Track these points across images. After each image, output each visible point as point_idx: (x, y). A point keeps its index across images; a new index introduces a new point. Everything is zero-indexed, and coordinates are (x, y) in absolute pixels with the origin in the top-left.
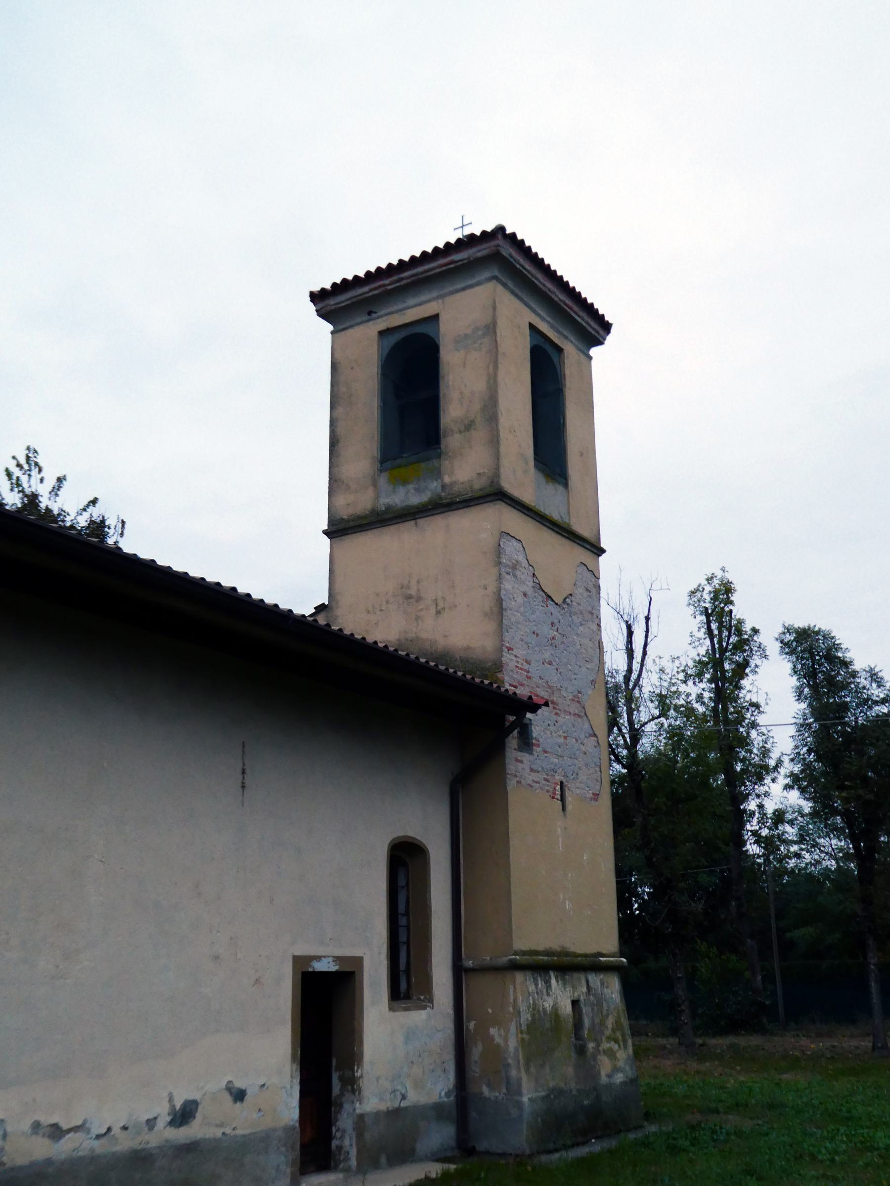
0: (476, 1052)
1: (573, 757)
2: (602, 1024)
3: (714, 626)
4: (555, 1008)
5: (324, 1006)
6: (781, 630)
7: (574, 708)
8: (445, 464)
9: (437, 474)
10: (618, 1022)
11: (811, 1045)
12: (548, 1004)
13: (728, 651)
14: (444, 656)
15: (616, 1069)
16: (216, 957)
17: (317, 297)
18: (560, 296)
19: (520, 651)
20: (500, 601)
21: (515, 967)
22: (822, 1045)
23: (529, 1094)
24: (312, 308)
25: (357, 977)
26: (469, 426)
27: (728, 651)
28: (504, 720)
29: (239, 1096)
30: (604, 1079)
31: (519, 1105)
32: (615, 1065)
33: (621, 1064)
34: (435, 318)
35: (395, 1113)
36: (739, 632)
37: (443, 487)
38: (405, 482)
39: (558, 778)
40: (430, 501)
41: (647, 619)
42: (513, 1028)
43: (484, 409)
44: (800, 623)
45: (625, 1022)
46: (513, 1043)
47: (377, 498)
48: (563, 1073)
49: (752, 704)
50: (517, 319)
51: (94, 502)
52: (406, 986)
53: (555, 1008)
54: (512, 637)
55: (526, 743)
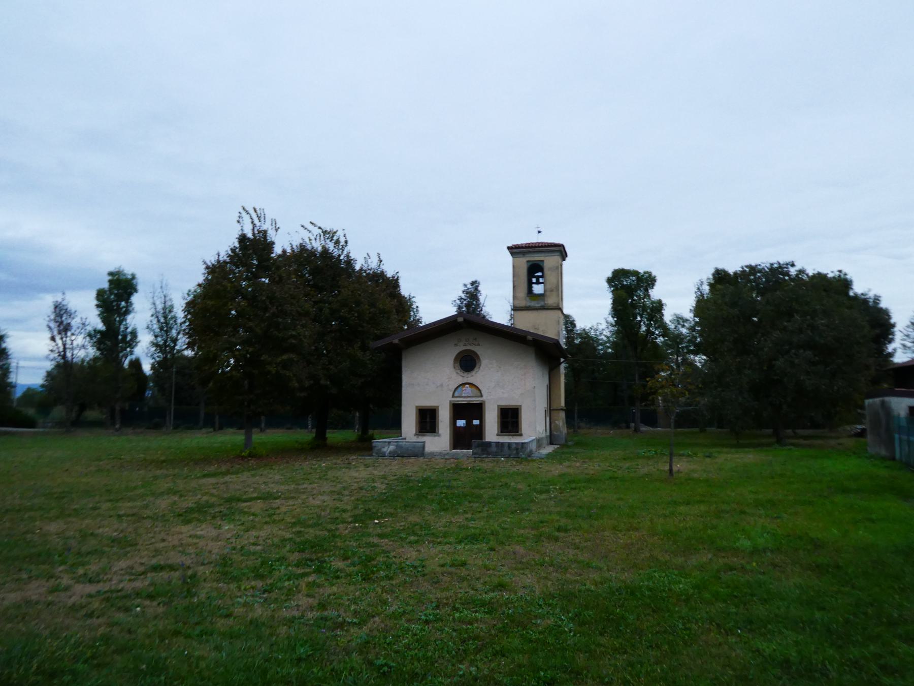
9: (544, 300)
38: (534, 300)
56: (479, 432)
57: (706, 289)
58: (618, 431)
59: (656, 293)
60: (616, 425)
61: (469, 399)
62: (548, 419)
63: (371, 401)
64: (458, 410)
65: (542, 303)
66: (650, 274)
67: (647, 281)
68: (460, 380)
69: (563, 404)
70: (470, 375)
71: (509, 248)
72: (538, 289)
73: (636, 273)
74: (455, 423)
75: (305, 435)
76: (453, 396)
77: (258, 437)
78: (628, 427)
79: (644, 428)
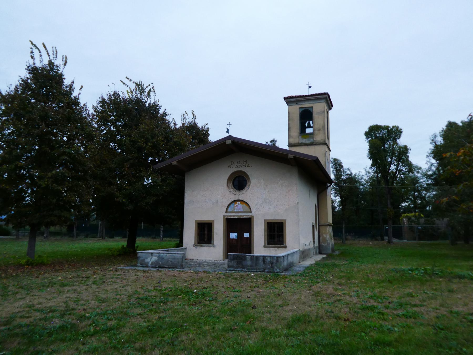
0: (321, 238)
9: (313, 138)
25: (198, 241)
26: (319, 130)
38: (305, 138)
43: (323, 127)
46: (328, 237)
56: (247, 245)
57: (440, 140)
58: (376, 242)
59: (402, 141)
60: (373, 237)
61: (240, 214)
62: (316, 233)
63: (164, 216)
64: (232, 224)
65: (311, 140)
66: (397, 128)
67: (395, 133)
68: (233, 198)
69: (330, 220)
70: (241, 193)
71: (285, 98)
72: (308, 131)
73: (387, 128)
74: (228, 235)
75: (120, 243)
77: (46, 247)
78: (383, 239)
79: (395, 240)
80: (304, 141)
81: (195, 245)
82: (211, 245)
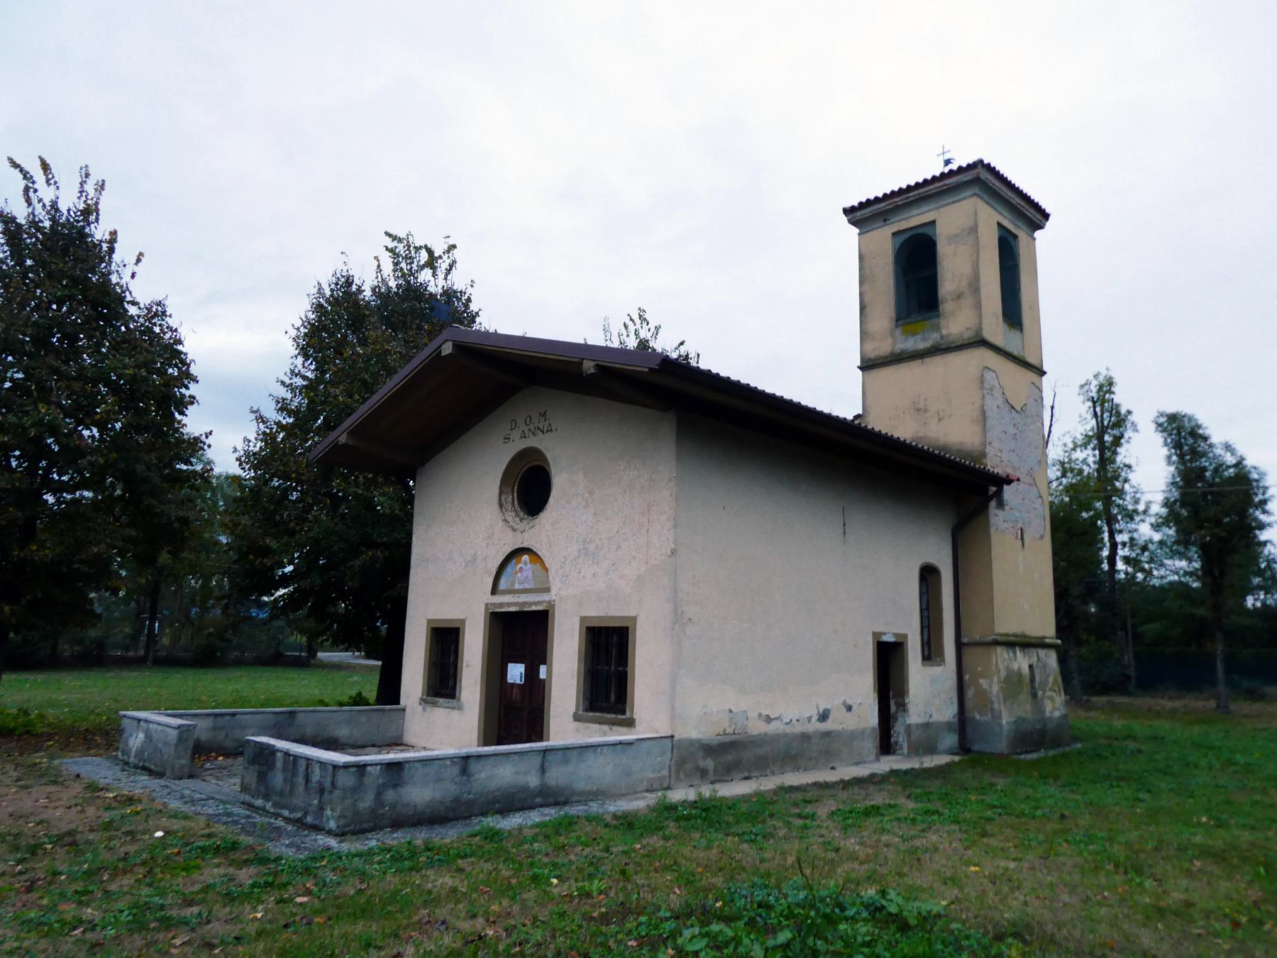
0: (970, 693)
1: (1028, 512)
2: (1046, 680)
3: (1098, 409)
4: (1019, 668)
5: (888, 658)
6: (1156, 414)
7: (1028, 480)
8: (943, 322)
9: (937, 328)
10: (1055, 680)
11: (1169, 704)
12: (1015, 666)
13: (1109, 426)
14: (945, 448)
15: (1054, 709)
16: (835, 631)
17: (846, 211)
18: (1017, 200)
19: (996, 444)
20: (983, 412)
21: (996, 643)
22: (1178, 704)
23: (1006, 719)
24: (845, 219)
26: (959, 296)
27: (1109, 426)
28: (987, 490)
29: (849, 708)
30: (1048, 714)
31: (1000, 725)
32: (1055, 705)
33: (1058, 705)
34: (933, 222)
35: (926, 726)
36: (1118, 413)
37: (942, 337)
38: (914, 334)
39: (1020, 525)
40: (932, 347)
41: (1052, 408)
42: (996, 680)
43: (970, 284)
44: (1171, 409)
45: (1060, 680)
46: (995, 688)
47: (895, 343)
48: (1024, 709)
49: (1126, 466)
50: (989, 218)
51: (682, 343)
52: (931, 653)
53: (1019, 668)
54: (993, 435)
55: (1001, 505)
74: (532, 673)
76: (494, 591)
80: (913, 344)
81: (423, 701)
82: (452, 702)
